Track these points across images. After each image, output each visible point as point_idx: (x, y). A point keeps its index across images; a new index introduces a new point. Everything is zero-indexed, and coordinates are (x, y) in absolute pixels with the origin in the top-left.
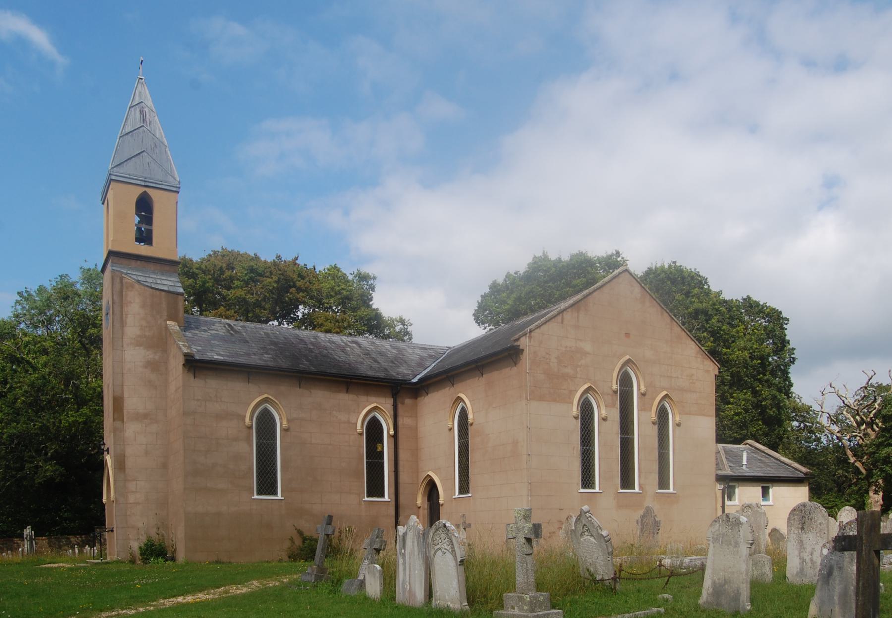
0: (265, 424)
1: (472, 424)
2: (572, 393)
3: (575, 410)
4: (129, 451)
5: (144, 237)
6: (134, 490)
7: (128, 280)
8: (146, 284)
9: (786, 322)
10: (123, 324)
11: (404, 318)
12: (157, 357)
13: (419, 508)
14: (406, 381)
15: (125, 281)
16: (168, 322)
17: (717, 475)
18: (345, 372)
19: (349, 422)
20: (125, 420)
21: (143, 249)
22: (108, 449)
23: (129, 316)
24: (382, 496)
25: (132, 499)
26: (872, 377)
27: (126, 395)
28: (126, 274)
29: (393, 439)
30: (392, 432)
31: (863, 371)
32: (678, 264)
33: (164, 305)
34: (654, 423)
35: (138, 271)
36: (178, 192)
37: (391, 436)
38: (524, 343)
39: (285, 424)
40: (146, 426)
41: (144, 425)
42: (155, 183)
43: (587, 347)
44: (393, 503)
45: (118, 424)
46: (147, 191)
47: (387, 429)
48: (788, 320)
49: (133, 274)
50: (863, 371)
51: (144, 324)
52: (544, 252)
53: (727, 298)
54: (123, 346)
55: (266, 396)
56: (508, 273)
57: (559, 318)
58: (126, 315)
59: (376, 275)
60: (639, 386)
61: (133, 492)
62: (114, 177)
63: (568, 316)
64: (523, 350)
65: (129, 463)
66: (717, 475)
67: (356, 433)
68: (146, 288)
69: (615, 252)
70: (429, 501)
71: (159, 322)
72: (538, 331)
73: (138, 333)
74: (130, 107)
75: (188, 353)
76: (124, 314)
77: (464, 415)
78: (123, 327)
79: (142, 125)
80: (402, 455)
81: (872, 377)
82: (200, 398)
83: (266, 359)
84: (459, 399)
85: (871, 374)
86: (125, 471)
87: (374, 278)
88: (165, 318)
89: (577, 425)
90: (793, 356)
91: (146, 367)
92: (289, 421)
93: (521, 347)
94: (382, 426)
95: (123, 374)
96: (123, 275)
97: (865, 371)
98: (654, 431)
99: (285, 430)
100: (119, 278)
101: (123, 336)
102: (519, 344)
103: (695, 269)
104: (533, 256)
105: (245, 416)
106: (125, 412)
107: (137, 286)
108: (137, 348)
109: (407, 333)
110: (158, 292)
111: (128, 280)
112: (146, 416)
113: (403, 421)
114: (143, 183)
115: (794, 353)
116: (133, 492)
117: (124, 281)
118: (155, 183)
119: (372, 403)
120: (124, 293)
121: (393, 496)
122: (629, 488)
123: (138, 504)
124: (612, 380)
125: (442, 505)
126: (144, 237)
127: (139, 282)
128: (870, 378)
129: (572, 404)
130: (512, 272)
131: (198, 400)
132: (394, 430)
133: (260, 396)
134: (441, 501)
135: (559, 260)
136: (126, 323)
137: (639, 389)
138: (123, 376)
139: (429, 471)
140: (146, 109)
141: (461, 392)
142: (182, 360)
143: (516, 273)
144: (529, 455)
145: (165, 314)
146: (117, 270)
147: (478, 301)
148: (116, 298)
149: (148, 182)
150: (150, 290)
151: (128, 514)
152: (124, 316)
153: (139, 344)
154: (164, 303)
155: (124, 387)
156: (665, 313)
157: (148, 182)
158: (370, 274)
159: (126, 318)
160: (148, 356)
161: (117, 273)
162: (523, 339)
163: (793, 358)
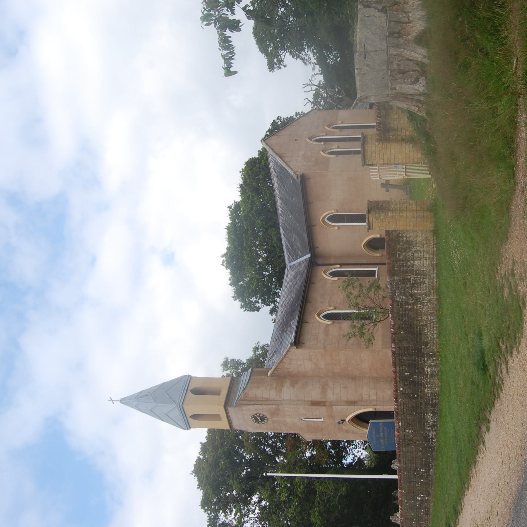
0: (328, 317)
1: (337, 212)
2: (324, 157)
3: (334, 156)
4: (344, 398)
5: (216, 393)
6: (368, 395)
7: (242, 397)
8: (245, 385)
9: (280, 118)
10: (268, 400)
11: (254, 347)
12: (289, 381)
13: (382, 255)
14: (309, 259)
15: (242, 398)
16: (269, 375)
17: (369, 108)
18: (299, 302)
19: (332, 283)
20: (325, 400)
21: (224, 392)
22: (342, 420)
23: (263, 396)
24: (375, 271)
25: (374, 397)
26: (308, 100)
27: (310, 399)
28: (238, 397)
29: (342, 266)
30: (338, 266)
31: (304, 106)
32: (241, 170)
33: (258, 377)
34: (341, 131)
35: (236, 393)
36: (191, 376)
37: (340, 267)
38: (299, 173)
39: (332, 308)
40: (329, 388)
41: (329, 389)
42: (186, 385)
43: (302, 153)
44: (379, 266)
45: (327, 404)
46: (190, 389)
47: (337, 268)
48: (279, 117)
49: (239, 392)
50: (304, 106)
51: (269, 387)
52: (220, 257)
53: (264, 136)
54: (281, 401)
55: (316, 316)
56: (229, 284)
57: (287, 162)
58: (263, 398)
59: (225, 357)
60: (322, 136)
61: (369, 396)
62: (181, 404)
63: (286, 159)
64: (303, 174)
65: (351, 398)
66: (369, 108)
67: (338, 281)
68: (248, 386)
69: (228, 209)
70: (378, 249)
71: (268, 380)
72: (293, 169)
73: (274, 391)
74: (138, 402)
75: (291, 344)
76: (261, 399)
77: (334, 219)
78: (269, 400)
79: (150, 395)
80: (352, 261)
81: (308, 100)
82: (316, 342)
83: (294, 324)
84: (323, 220)
85: (307, 101)
86: (356, 401)
87: (227, 359)
88: (266, 377)
89: (341, 157)
90: (300, 113)
91: (294, 387)
92: (330, 306)
93: (301, 174)
94: (330, 313)
95: (297, 401)
96: (239, 399)
97: (305, 105)
98: (345, 131)
99: (335, 309)
100: (241, 402)
101: (275, 400)
102: (300, 175)
103: (244, 164)
104: (222, 266)
105: (327, 324)
106: (320, 400)
107: (246, 391)
108: (283, 392)
109: (263, 347)
110: (251, 380)
111: (242, 397)
112: (323, 388)
113: (332, 261)
114: (185, 391)
115: (299, 113)
116: (369, 396)
117: (242, 399)
118: (186, 385)
119: (321, 274)
120: (250, 399)
121: (375, 266)
122: (375, 272)
123: (376, 393)
124: (318, 145)
125: (381, 235)
126: (216, 393)
127: (244, 390)
128: (308, 101)
129: (330, 157)
130: (229, 282)
131: (317, 343)
132: (337, 265)
133: (315, 318)
134: (378, 236)
135: (228, 249)
136: (268, 398)
137: (324, 136)
138: (299, 401)
139: (361, 247)
140: (140, 395)
141: (320, 221)
142: (294, 349)
143: (230, 280)
144: (355, 171)
145: (264, 377)
146: (236, 402)
147: (244, 311)
148: (252, 403)
149: (185, 388)
150: (249, 384)
151: (383, 400)
152: (263, 399)
153: (281, 391)
154: (257, 377)
155: (305, 400)
156: (286, 128)
157: (185, 388)
158: (224, 361)
159: (264, 398)
160: (288, 386)
161: (237, 402)
162: (297, 174)
163: (301, 113)
